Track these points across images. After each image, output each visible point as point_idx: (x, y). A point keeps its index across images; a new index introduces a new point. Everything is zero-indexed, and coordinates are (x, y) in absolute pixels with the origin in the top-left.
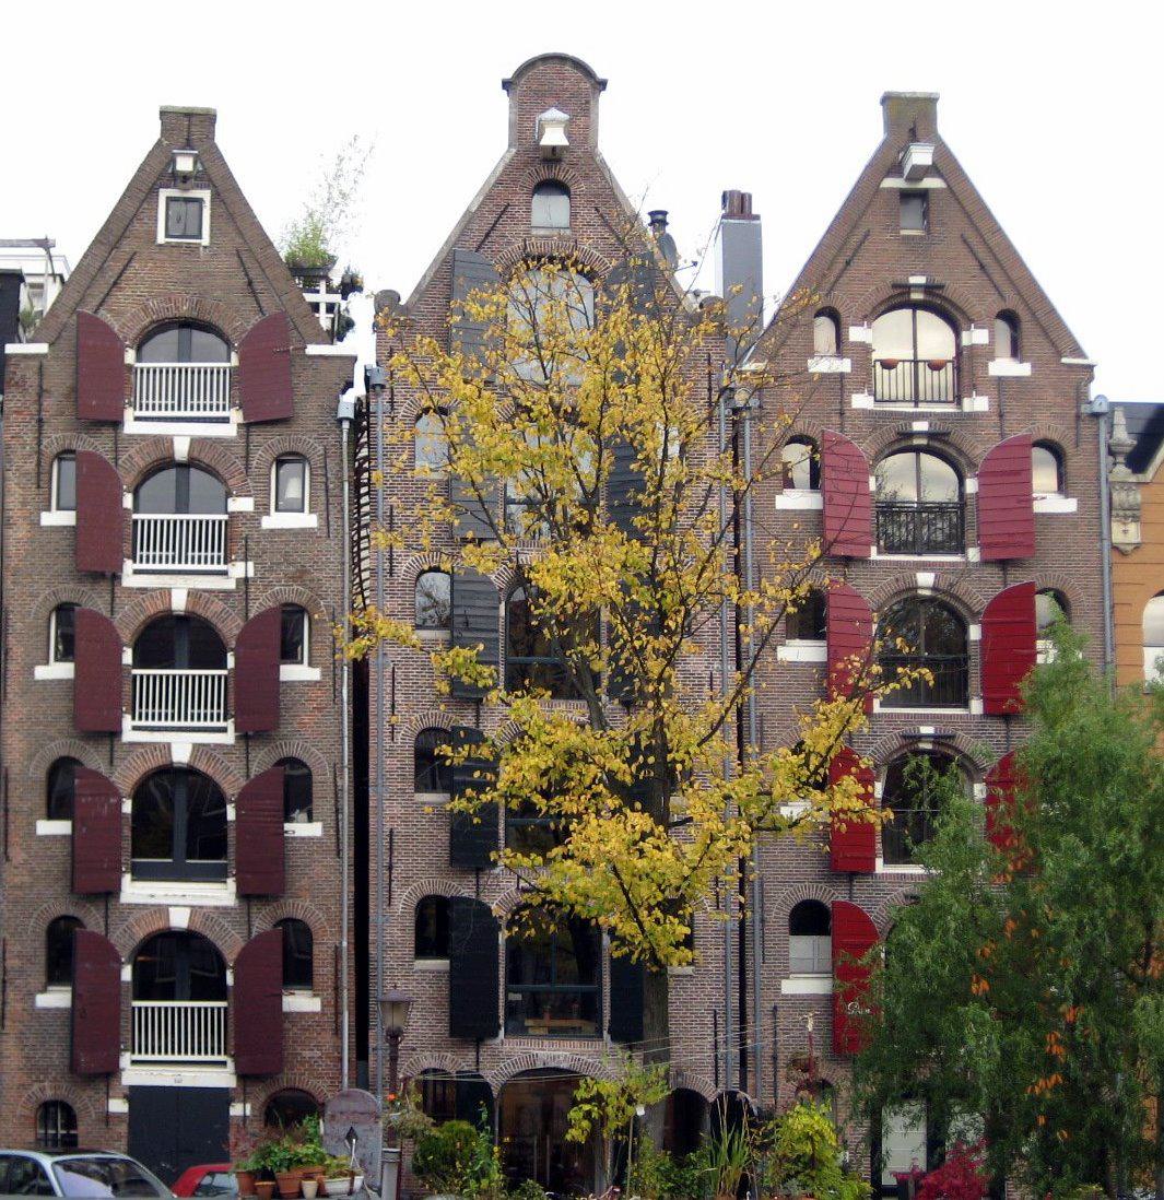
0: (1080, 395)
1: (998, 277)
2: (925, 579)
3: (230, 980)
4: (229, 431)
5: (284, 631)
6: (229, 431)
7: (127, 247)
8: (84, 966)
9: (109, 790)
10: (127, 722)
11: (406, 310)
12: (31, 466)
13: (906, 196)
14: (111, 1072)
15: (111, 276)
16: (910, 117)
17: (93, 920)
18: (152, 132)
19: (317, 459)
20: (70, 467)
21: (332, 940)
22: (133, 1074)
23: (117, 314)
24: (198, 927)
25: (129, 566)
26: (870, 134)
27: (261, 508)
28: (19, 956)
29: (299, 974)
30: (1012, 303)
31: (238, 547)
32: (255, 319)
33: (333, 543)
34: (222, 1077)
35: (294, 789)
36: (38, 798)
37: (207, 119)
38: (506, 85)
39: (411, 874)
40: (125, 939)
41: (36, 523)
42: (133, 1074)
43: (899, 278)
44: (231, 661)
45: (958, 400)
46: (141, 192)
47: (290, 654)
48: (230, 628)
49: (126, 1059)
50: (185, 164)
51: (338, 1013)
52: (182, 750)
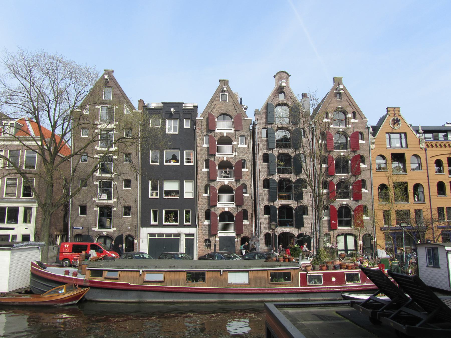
0: (365, 125)
1: (352, 106)
2: (342, 154)
3: (235, 219)
4: (232, 131)
5: (242, 164)
6: (232, 131)
7: (215, 102)
8: (212, 217)
9: (216, 215)
10: (217, 178)
11: (260, 112)
12: (201, 137)
13: (337, 93)
14: (216, 234)
15: (213, 107)
16: (337, 81)
17: (213, 210)
18: (218, 84)
19: (246, 136)
20: (207, 138)
21: (250, 212)
22: (220, 234)
23: (214, 113)
24: (230, 211)
25: (217, 153)
26: (331, 85)
27: (238, 144)
28: (201, 216)
29: (246, 218)
30: (355, 110)
31: (234, 150)
32: (236, 114)
33: (249, 149)
34: (234, 235)
35: (244, 215)
36: (203, 190)
37: (228, 81)
38: (275, 76)
39: (264, 202)
40: (218, 213)
41: (202, 146)
42: (220, 234)
43: (337, 107)
44: (234, 168)
45: (346, 126)
46: (217, 93)
47: (244, 167)
48: (234, 163)
49: (218, 232)
50: (225, 89)
51: (252, 224)
52: (225, 133)
